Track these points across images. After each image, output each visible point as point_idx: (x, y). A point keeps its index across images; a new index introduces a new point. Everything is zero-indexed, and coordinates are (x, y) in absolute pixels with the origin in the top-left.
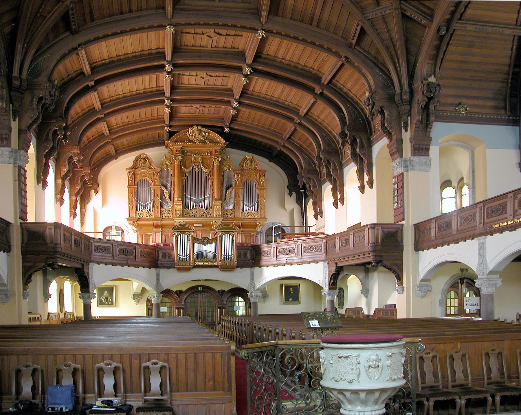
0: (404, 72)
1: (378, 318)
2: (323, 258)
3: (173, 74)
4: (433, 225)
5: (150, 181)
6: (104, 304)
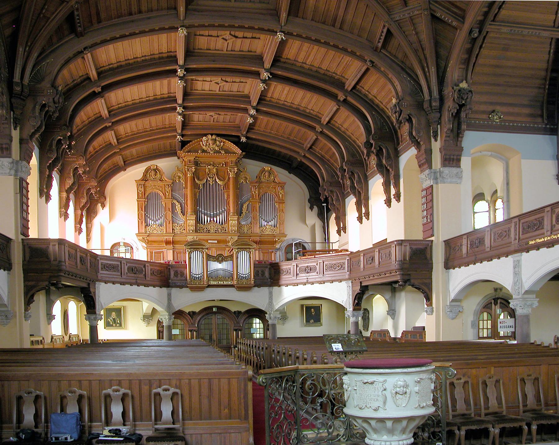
0: (434, 77)
1: (405, 341)
2: (347, 277)
3: (186, 80)
4: (464, 242)
5: (161, 194)
6: (112, 326)
